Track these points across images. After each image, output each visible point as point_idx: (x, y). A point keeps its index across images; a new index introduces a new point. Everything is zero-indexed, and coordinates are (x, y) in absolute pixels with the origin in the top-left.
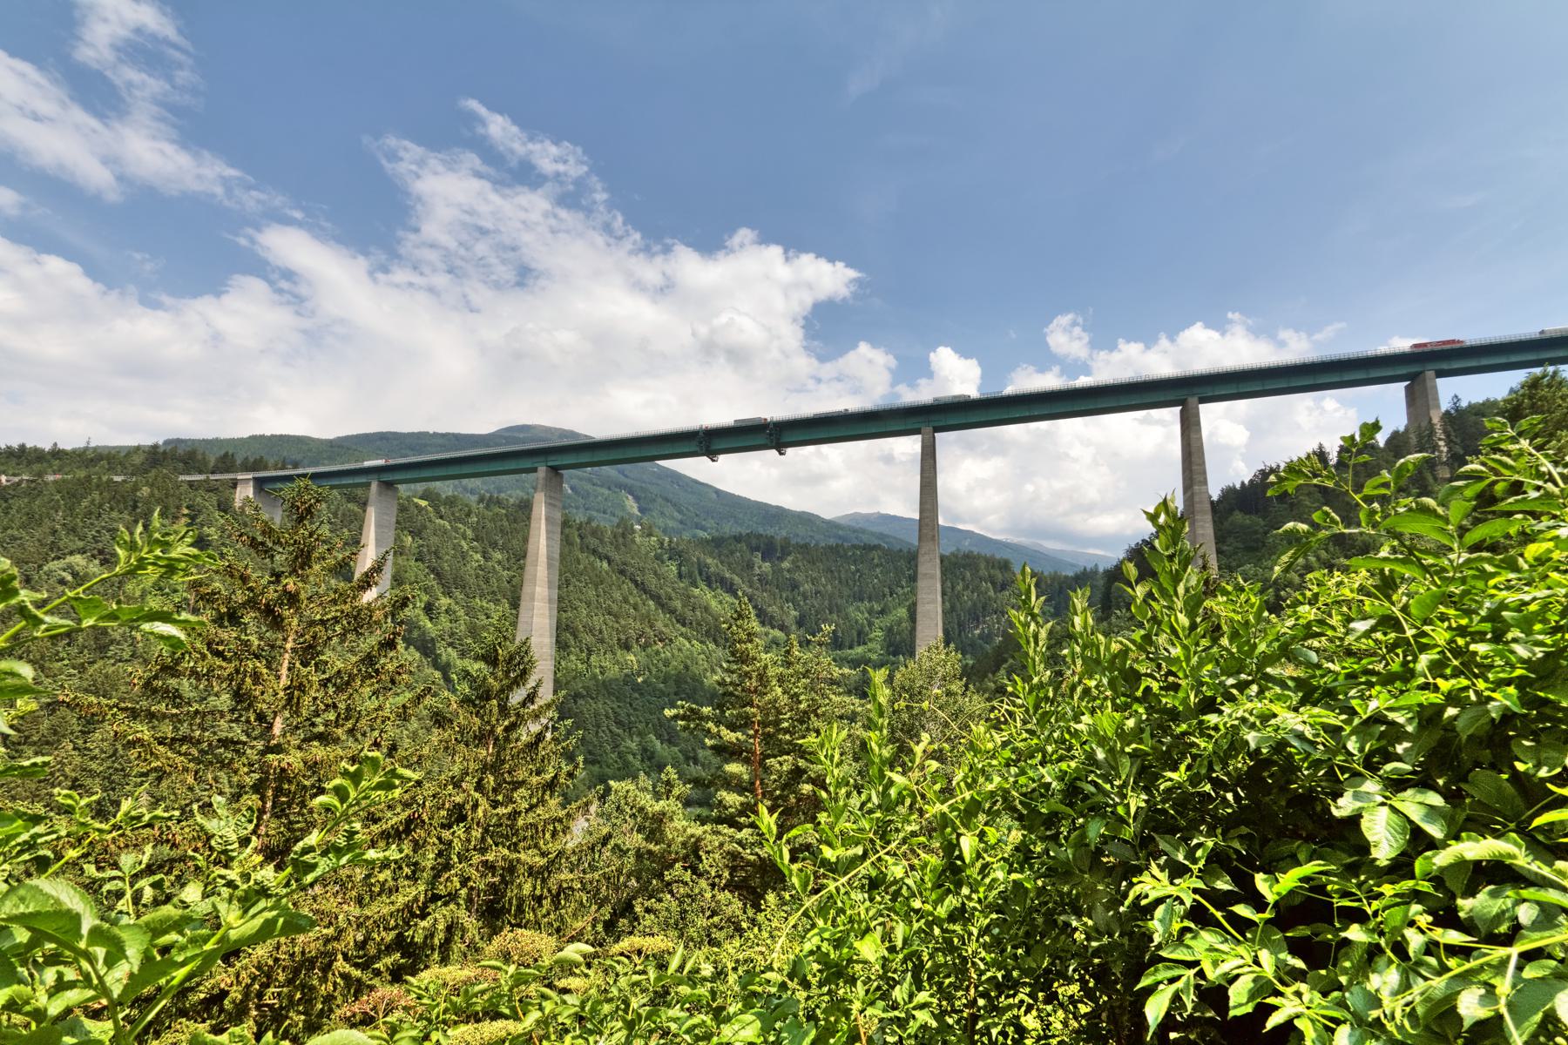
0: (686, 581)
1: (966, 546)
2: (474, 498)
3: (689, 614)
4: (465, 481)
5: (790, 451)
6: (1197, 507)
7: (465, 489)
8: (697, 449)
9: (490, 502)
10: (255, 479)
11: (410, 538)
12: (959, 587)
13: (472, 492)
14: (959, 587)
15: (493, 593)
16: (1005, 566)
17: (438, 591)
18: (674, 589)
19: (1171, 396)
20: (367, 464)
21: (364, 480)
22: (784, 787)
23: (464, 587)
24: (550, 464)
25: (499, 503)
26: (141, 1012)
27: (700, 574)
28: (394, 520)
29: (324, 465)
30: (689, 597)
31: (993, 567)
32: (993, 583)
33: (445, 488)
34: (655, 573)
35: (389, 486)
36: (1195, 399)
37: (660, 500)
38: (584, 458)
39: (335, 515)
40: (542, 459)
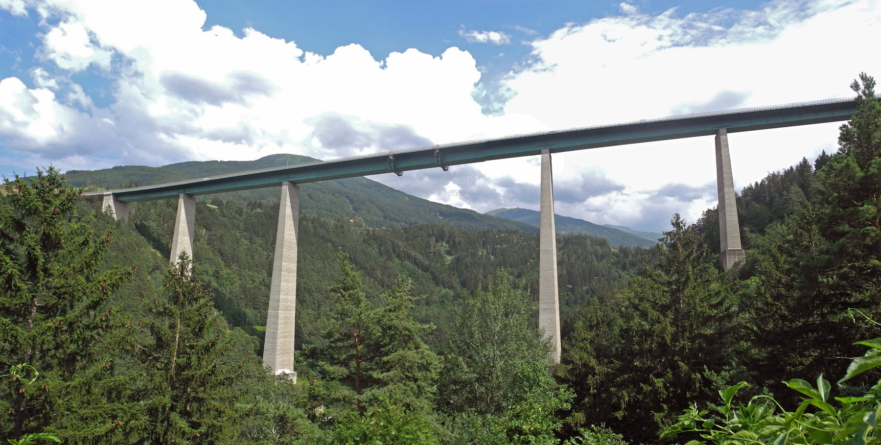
0: (384, 258)
1: (578, 231)
2: (246, 203)
3: (386, 279)
4: (240, 192)
5: (405, 173)
6: (727, 202)
7: (240, 197)
8: (388, 168)
9: (253, 205)
10: (113, 194)
11: (204, 230)
12: (573, 258)
13: (245, 199)
14: (573, 258)
15: (257, 266)
16: (603, 243)
17: (222, 264)
18: (376, 263)
19: (708, 128)
20: (205, 179)
21: (175, 194)
22: (604, 355)
23: (237, 262)
24: (290, 180)
25: (260, 206)
26: (854, 252)
27: (394, 252)
28: (194, 219)
29: (155, 184)
30: (386, 268)
31: (596, 244)
32: (596, 256)
33: (224, 197)
34: (363, 252)
35: (190, 196)
36: (725, 130)
37: (367, 202)
38: (313, 176)
39: (159, 215)
40: (182, 191)
